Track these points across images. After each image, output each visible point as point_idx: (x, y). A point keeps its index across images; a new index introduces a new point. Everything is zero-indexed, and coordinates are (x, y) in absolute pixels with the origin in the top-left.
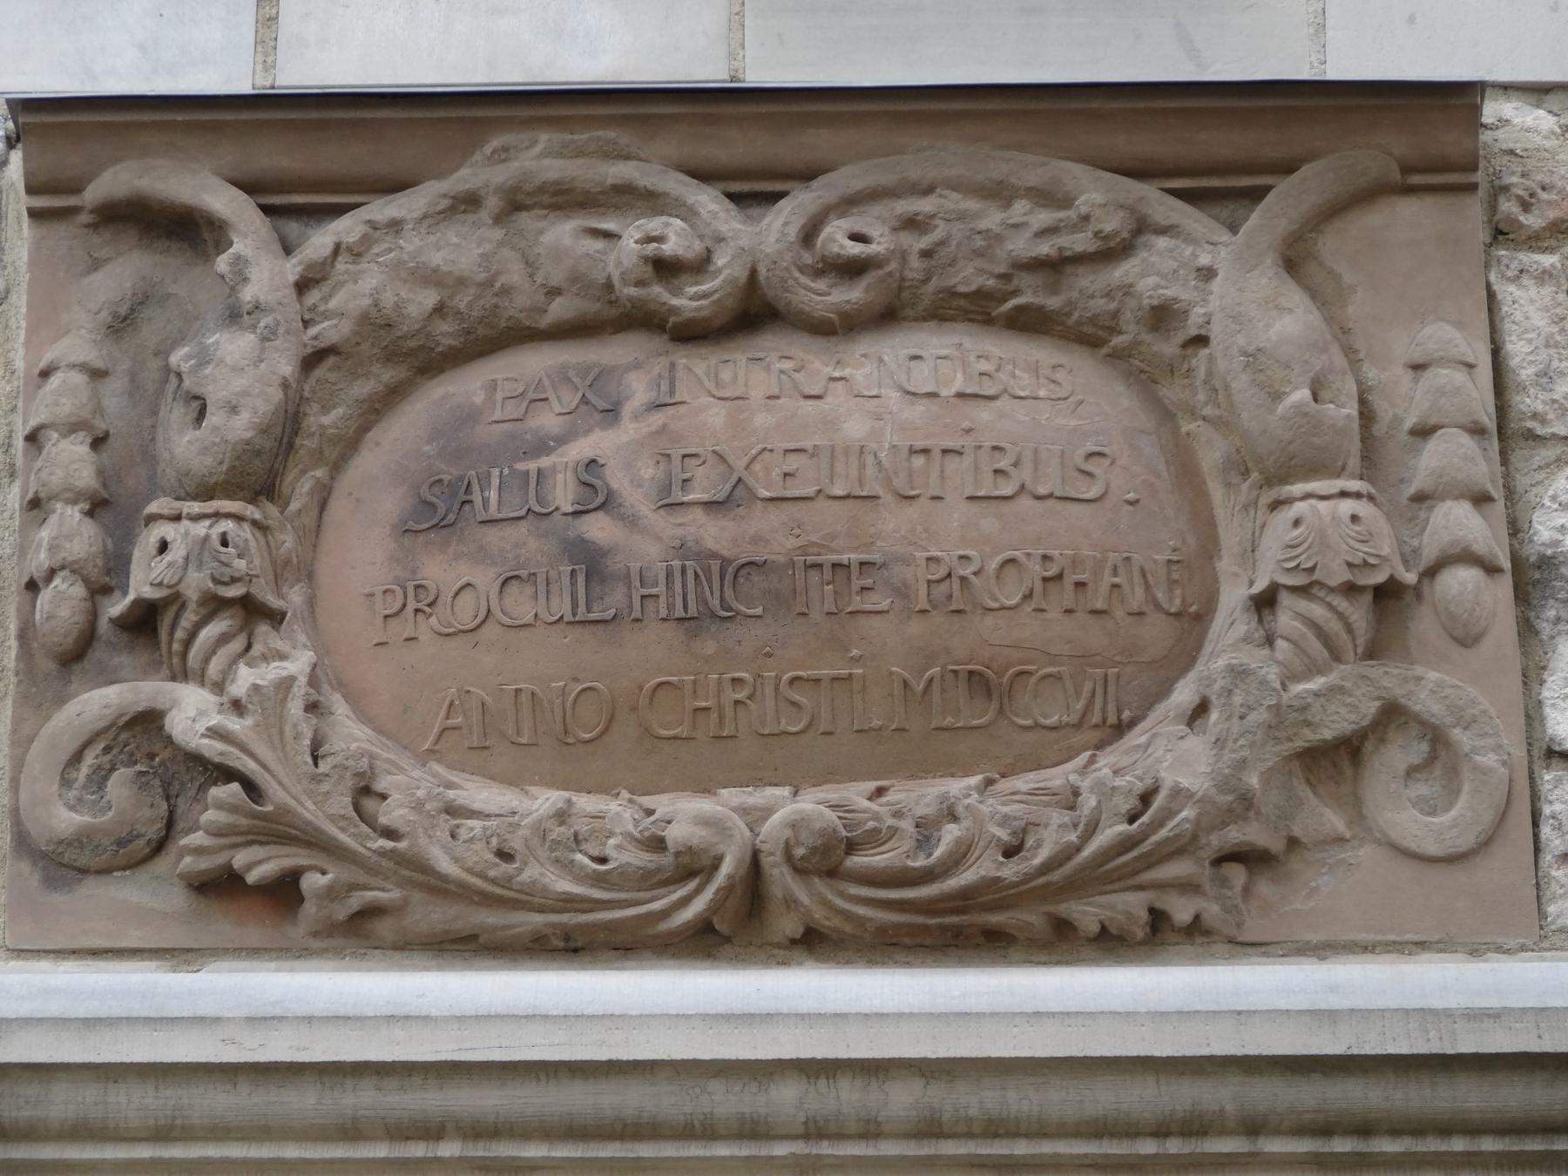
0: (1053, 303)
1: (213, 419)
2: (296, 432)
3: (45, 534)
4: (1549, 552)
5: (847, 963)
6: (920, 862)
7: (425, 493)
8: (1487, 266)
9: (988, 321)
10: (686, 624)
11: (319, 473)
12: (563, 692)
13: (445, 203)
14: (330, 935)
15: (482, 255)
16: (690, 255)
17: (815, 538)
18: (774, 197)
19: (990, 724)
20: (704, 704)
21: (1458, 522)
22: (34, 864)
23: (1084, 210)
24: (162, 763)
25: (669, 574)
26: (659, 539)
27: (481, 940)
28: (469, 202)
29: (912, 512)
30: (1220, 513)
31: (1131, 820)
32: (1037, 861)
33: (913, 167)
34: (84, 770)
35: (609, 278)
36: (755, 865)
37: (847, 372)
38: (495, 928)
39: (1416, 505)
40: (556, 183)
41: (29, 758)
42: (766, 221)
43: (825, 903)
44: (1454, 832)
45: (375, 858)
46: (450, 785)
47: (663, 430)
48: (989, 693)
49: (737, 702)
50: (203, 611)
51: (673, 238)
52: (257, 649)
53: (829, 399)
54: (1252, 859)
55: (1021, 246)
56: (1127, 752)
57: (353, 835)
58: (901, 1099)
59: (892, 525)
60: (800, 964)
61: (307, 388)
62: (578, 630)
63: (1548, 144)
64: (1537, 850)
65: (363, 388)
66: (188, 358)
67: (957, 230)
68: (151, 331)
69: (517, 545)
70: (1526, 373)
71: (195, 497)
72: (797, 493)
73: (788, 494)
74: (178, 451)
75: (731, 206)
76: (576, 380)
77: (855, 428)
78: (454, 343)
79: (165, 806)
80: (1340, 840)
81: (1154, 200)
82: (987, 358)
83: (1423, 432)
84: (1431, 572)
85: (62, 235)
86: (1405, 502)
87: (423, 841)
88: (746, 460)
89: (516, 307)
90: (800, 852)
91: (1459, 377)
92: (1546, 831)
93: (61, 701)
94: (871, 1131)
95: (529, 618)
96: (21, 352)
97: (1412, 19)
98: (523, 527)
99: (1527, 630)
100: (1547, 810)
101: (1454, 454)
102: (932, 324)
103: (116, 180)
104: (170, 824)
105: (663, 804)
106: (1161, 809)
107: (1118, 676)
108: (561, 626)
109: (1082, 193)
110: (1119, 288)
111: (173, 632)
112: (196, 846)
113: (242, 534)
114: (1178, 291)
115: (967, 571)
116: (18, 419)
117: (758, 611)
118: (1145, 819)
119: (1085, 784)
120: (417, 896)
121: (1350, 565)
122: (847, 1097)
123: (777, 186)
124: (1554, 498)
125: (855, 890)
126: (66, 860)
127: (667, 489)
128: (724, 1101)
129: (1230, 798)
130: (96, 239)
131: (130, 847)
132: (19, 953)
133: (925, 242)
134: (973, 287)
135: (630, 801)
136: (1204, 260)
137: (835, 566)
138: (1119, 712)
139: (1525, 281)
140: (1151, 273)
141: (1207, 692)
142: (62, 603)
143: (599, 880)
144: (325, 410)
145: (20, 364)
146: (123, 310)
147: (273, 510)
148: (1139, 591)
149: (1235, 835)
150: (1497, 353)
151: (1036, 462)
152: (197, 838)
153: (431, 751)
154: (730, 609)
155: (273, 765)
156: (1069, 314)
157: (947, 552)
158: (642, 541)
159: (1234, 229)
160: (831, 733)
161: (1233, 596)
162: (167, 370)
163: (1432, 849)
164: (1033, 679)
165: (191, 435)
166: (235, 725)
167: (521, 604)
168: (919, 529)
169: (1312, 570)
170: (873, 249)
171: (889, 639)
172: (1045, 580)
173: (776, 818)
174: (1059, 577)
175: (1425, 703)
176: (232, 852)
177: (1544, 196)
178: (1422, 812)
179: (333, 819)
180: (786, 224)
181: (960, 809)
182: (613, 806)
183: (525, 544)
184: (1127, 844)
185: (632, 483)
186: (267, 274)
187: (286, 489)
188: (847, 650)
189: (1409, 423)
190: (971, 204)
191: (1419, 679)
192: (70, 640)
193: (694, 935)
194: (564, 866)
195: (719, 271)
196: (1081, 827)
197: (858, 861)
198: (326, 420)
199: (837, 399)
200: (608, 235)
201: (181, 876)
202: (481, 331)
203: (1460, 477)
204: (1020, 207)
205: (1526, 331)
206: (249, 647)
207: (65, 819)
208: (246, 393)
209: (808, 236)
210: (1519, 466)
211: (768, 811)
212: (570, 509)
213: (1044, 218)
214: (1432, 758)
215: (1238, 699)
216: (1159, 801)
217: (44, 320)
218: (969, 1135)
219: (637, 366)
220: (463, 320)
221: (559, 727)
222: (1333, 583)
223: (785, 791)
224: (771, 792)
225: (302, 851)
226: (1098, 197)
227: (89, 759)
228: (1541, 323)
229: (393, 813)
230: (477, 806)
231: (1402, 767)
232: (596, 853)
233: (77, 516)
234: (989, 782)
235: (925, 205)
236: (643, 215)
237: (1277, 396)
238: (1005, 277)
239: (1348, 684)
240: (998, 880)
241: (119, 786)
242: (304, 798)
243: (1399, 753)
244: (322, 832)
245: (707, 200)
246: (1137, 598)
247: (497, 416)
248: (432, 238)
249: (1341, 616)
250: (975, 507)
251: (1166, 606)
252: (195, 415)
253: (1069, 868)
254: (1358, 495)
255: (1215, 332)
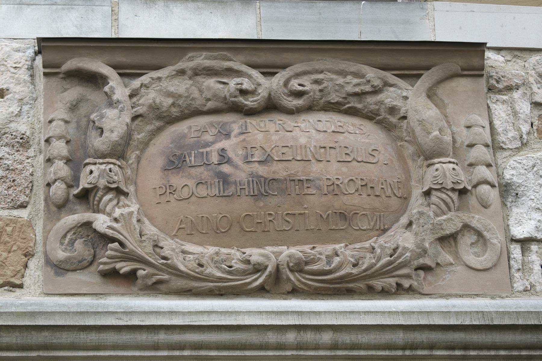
0: (359, 106)
1: (106, 134)
2: (130, 140)
3: (52, 169)
4: (509, 182)
5: (305, 299)
6: (328, 268)
7: (172, 159)
8: (487, 99)
9: (340, 112)
10: (254, 197)
11: (137, 152)
12: (216, 217)
13: (174, 73)
14: (145, 290)
15: (186, 88)
16: (250, 89)
17: (292, 172)
18: (274, 74)
19: (346, 228)
20: (260, 221)
21: (482, 172)
22: (52, 268)
23: (368, 79)
24: (91, 238)
25: (248, 182)
26: (244, 172)
27: (193, 291)
28: (182, 72)
29: (321, 165)
30: (412, 169)
31: (391, 256)
32: (363, 268)
33: (317, 65)
34: (67, 240)
35: (225, 96)
36: (278, 269)
37: (299, 125)
38: (198, 287)
39: (469, 167)
40: (208, 67)
41: (49, 236)
42: (273, 80)
43: (299, 280)
44: (485, 262)
45: (160, 266)
46: (182, 245)
47: (244, 140)
48: (346, 220)
49: (270, 221)
50: (104, 191)
51: (245, 84)
52: (121, 203)
53: (294, 132)
54: (426, 268)
55: (350, 89)
56: (388, 237)
57: (153, 259)
58: (327, 337)
59: (316, 169)
60: (290, 299)
61: (133, 126)
62: (220, 198)
63: (502, 65)
64: (510, 268)
65: (149, 128)
66: (97, 116)
67: (330, 84)
68: (83, 109)
69: (201, 174)
70: (500, 130)
71: (100, 158)
72: (286, 159)
73: (284, 159)
74: (95, 144)
75: (262, 75)
76: (216, 126)
77: (303, 141)
78: (178, 115)
79: (93, 251)
80: (451, 264)
81: (389, 76)
82: (340, 122)
83: (471, 146)
84: (475, 186)
85: (54, 82)
86: (466, 166)
87: (175, 260)
88: (270, 149)
89: (198, 103)
90: (291, 264)
91: (481, 130)
92: (512, 262)
93: (59, 219)
94: (317, 347)
95: (205, 195)
96: (42, 116)
97: (460, 28)
98: (202, 168)
99: (504, 204)
100: (512, 256)
101: (480, 152)
102: (323, 112)
103: (72, 64)
104: (94, 256)
105: (248, 251)
106: (399, 253)
107: (384, 215)
108: (216, 197)
109: (367, 74)
110: (379, 102)
111: (94, 199)
112: (104, 261)
113: (116, 169)
114: (398, 103)
115: (338, 183)
116: (42, 136)
117: (276, 193)
118: (395, 256)
119: (376, 246)
120: (173, 278)
121: (453, 182)
122: (309, 337)
123: (275, 70)
124: (510, 166)
125: (308, 276)
126: (62, 267)
127: (247, 157)
128: (272, 337)
129: (420, 250)
130: (64, 82)
131: (83, 263)
132: (48, 294)
133: (320, 87)
134: (336, 101)
135: (238, 250)
136: (405, 94)
137: (299, 180)
138: (384, 226)
139: (498, 103)
140: (390, 97)
141: (412, 219)
142: (59, 190)
143: (229, 273)
144: (139, 134)
145: (42, 119)
146: (74, 103)
147: (124, 163)
148: (390, 190)
149: (421, 261)
150: (491, 123)
151: (358, 151)
152: (104, 260)
153: (175, 235)
154: (267, 193)
155: (128, 237)
156: (364, 110)
157: (333, 177)
158: (240, 174)
159: (413, 86)
160: (298, 230)
161: (417, 192)
162: (89, 121)
163: (479, 267)
164: (359, 215)
165: (99, 139)
166: (115, 225)
167: (202, 191)
168: (324, 170)
169: (442, 184)
170: (305, 88)
171: (315, 201)
172: (362, 186)
173: (284, 254)
174: (366, 185)
175: (474, 223)
176: (115, 264)
177: (503, 79)
178: (475, 256)
179: (147, 253)
180: (279, 80)
181: (339, 253)
182: (233, 251)
183: (204, 173)
184: (389, 263)
185: (236, 154)
186: (120, 92)
187: (128, 157)
188: (303, 205)
189: (466, 143)
190: (334, 76)
191: (473, 217)
192: (61, 201)
193: (258, 291)
194: (219, 269)
195: (259, 94)
196: (376, 258)
197: (308, 268)
198: (139, 137)
199: (297, 133)
200: (224, 83)
201: (99, 272)
202: (186, 111)
203: (483, 159)
204: (349, 77)
205: (499, 118)
206: (118, 203)
207: (61, 254)
208: (115, 127)
209: (286, 84)
210: (499, 157)
211: (281, 253)
212: (217, 163)
213: (356, 81)
214: (477, 241)
215: (422, 221)
216: (399, 250)
217: (49, 105)
218: (346, 349)
219: (234, 122)
220: (181, 108)
221: (215, 228)
222: (449, 188)
223: (286, 247)
224: (283, 247)
225: (139, 264)
226: (373, 75)
227: (69, 236)
228: (504, 115)
229: (166, 252)
230: (191, 251)
231: (469, 243)
232: (229, 264)
233: (62, 164)
234: (347, 246)
235: (320, 76)
236: (235, 77)
237: (429, 133)
238: (345, 98)
239: (453, 218)
240: (352, 273)
241: (79, 244)
242: (138, 247)
243: (468, 239)
244: (144, 258)
245: (255, 73)
246: (389, 192)
247: (192, 136)
248: (170, 83)
249: (450, 197)
250: (340, 164)
251: (397, 195)
252: (99, 133)
253: (373, 270)
254: (454, 163)
255: (410, 115)
